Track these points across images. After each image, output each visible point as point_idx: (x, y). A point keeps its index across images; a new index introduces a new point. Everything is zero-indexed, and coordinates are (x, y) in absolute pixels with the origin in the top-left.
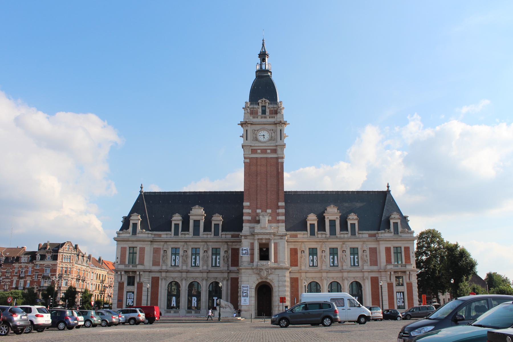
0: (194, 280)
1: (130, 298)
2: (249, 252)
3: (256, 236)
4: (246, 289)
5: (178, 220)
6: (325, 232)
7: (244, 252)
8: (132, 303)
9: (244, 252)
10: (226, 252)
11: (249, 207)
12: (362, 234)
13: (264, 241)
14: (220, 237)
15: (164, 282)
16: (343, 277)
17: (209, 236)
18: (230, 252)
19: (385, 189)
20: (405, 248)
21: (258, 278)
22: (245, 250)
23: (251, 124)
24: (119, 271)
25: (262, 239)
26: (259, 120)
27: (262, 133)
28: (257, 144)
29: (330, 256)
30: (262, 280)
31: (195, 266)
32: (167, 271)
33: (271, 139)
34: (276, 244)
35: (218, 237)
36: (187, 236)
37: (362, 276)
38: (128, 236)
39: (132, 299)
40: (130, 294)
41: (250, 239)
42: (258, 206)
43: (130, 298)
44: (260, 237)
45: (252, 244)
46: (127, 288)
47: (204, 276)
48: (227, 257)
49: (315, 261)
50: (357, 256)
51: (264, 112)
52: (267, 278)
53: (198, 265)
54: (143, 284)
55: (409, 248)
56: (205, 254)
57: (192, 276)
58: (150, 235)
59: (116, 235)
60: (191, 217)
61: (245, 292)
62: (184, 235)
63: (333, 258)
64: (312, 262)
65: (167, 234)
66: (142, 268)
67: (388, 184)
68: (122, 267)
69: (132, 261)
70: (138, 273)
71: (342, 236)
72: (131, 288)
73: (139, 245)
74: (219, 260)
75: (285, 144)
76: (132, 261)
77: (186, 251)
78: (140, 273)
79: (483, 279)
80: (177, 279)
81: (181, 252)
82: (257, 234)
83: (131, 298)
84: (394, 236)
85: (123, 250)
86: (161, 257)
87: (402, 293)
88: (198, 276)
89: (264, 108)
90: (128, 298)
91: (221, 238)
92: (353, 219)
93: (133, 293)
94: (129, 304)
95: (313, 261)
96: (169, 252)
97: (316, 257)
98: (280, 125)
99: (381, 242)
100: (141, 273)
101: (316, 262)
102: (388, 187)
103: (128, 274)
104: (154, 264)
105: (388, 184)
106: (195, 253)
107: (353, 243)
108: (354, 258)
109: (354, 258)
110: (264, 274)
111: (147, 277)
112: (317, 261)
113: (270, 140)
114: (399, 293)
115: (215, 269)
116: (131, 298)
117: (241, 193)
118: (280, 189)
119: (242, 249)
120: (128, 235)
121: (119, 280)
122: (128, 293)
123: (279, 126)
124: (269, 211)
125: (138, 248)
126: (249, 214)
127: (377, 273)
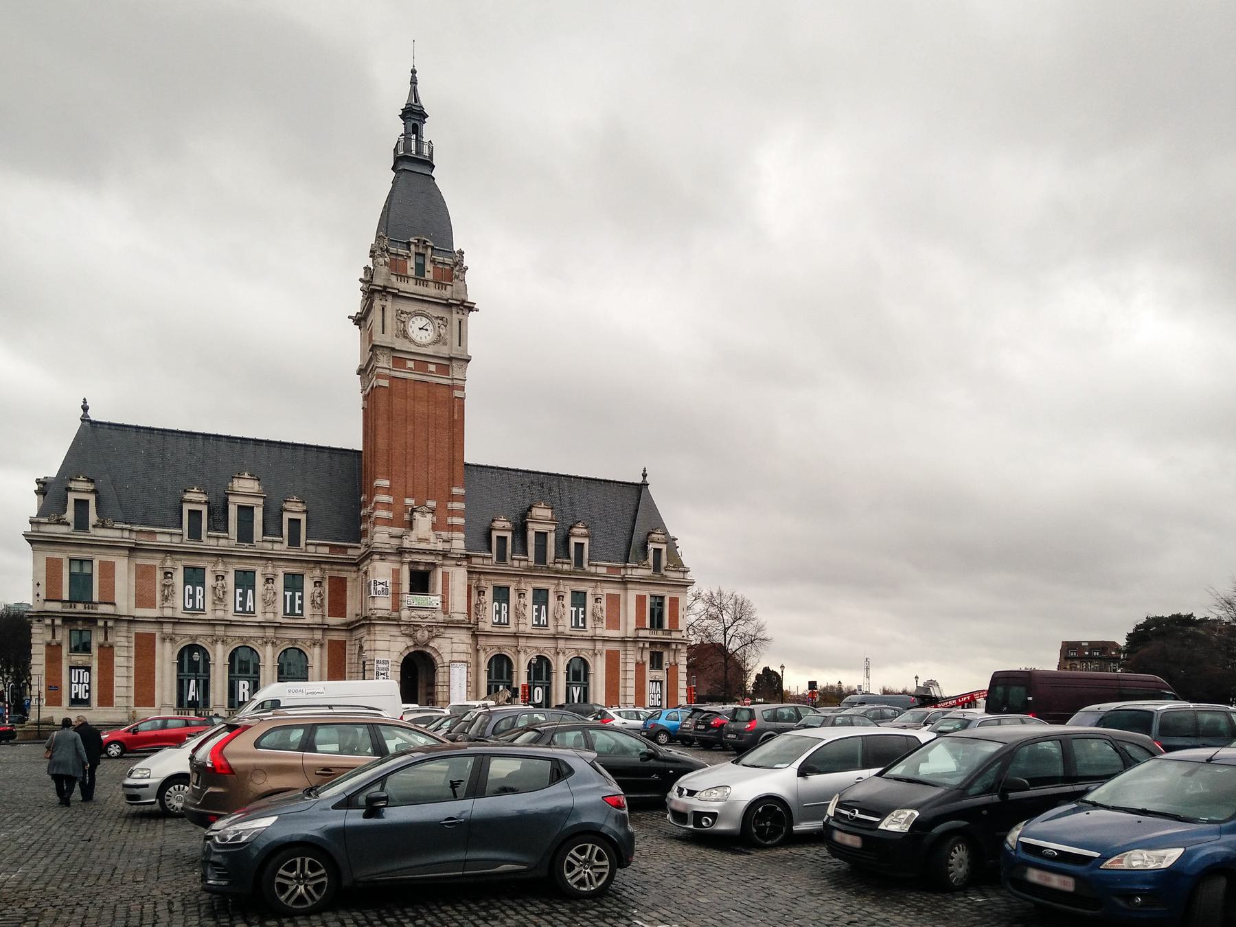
0: (244, 643)
1: (78, 683)
2: (390, 590)
3: (407, 555)
4: (385, 666)
5: (199, 503)
6: (227, 534)
7: (379, 588)
8: (87, 694)
9: (379, 588)
10: (317, 584)
11: (388, 491)
12: (597, 565)
13: (421, 568)
14: (304, 551)
15: (168, 645)
16: (556, 648)
17: (277, 546)
18: (326, 585)
19: (639, 480)
20: (671, 599)
21: (411, 643)
22: (380, 584)
23: (395, 296)
24: (49, 616)
25: (418, 563)
26: (410, 287)
27: (420, 322)
28: (406, 345)
29: (237, 590)
30: (416, 649)
31: (244, 611)
32: (177, 622)
33: (439, 340)
34: (445, 575)
35: (297, 550)
36: (222, 542)
37: (592, 647)
38: (67, 532)
39: (84, 685)
40: (79, 673)
41: (392, 562)
42: (410, 490)
43: (78, 683)
44: (416, 558)
45: (396, 573)
46: (650, 674)
47: (316, 637)
48: (320, 595)
49: (199, 597)
50: (583, 609)
51: (420, 269)
52: (427, 645)
53: (252, 610)
54: (115, 649)
55: (678, 601)
56: (270, 586)
57: (238, 634)
58: (126, 534)
59: (28, 528)
60: (530, 525)
61: (383, 672)
62: (215, 540)
63: (538, 610)
64: (191, 600)
65: (130, 531)
66: (112, 612)
67: (645, 471)
68: (56, 607)
69: (657, 623)
70: (101, 623)
71: (559, 566)
72: (80, 658)
73: (98, 557)
74: (300, 602)
75: (470, 356)
76: (657, 623)
77: (223, 577)
78: (106, 623)
79: (1053, 667)
80: (299, 643)
81: (210, 580)
82: (411, 552)
83: (82, 681)
84: (287, 550)
85: (53, 568)
86: (158, 587)
87: (658, 683)
88: (252, 635)
89: (420, 260)
90: (73, 681)
91: (306, 551)
92: (504, 529)
93: (88, 669)
94: (77, 695)
95: (193, 596)
96: (179, 578)
97: (201, 589)
98: (460, 309)
99: (629, 586)
100: (110, 624)
101: (202, 599)
102: (644, 476)
103: (71, 626)
104: (139, 604)
105: (645, 471)
106: (293, 582)
107: (578, 583)
108: (577, 612)
109: (577, 612)
110: (422, 635)
111: (125, 634)
112: (204, 597)
113: (435, 342)
114: (654, 683)
115: (538, 632)
116: (83, 683)
117: (361, 452)
118: (457, 455)
119: (375, 582)
120: (62, 529)
121: (639, 658)
122: (73, 670)
123: (458, 313)
124: (432, 504)
125: (96, 563)
126: (388, 506)
127: (617, 644)
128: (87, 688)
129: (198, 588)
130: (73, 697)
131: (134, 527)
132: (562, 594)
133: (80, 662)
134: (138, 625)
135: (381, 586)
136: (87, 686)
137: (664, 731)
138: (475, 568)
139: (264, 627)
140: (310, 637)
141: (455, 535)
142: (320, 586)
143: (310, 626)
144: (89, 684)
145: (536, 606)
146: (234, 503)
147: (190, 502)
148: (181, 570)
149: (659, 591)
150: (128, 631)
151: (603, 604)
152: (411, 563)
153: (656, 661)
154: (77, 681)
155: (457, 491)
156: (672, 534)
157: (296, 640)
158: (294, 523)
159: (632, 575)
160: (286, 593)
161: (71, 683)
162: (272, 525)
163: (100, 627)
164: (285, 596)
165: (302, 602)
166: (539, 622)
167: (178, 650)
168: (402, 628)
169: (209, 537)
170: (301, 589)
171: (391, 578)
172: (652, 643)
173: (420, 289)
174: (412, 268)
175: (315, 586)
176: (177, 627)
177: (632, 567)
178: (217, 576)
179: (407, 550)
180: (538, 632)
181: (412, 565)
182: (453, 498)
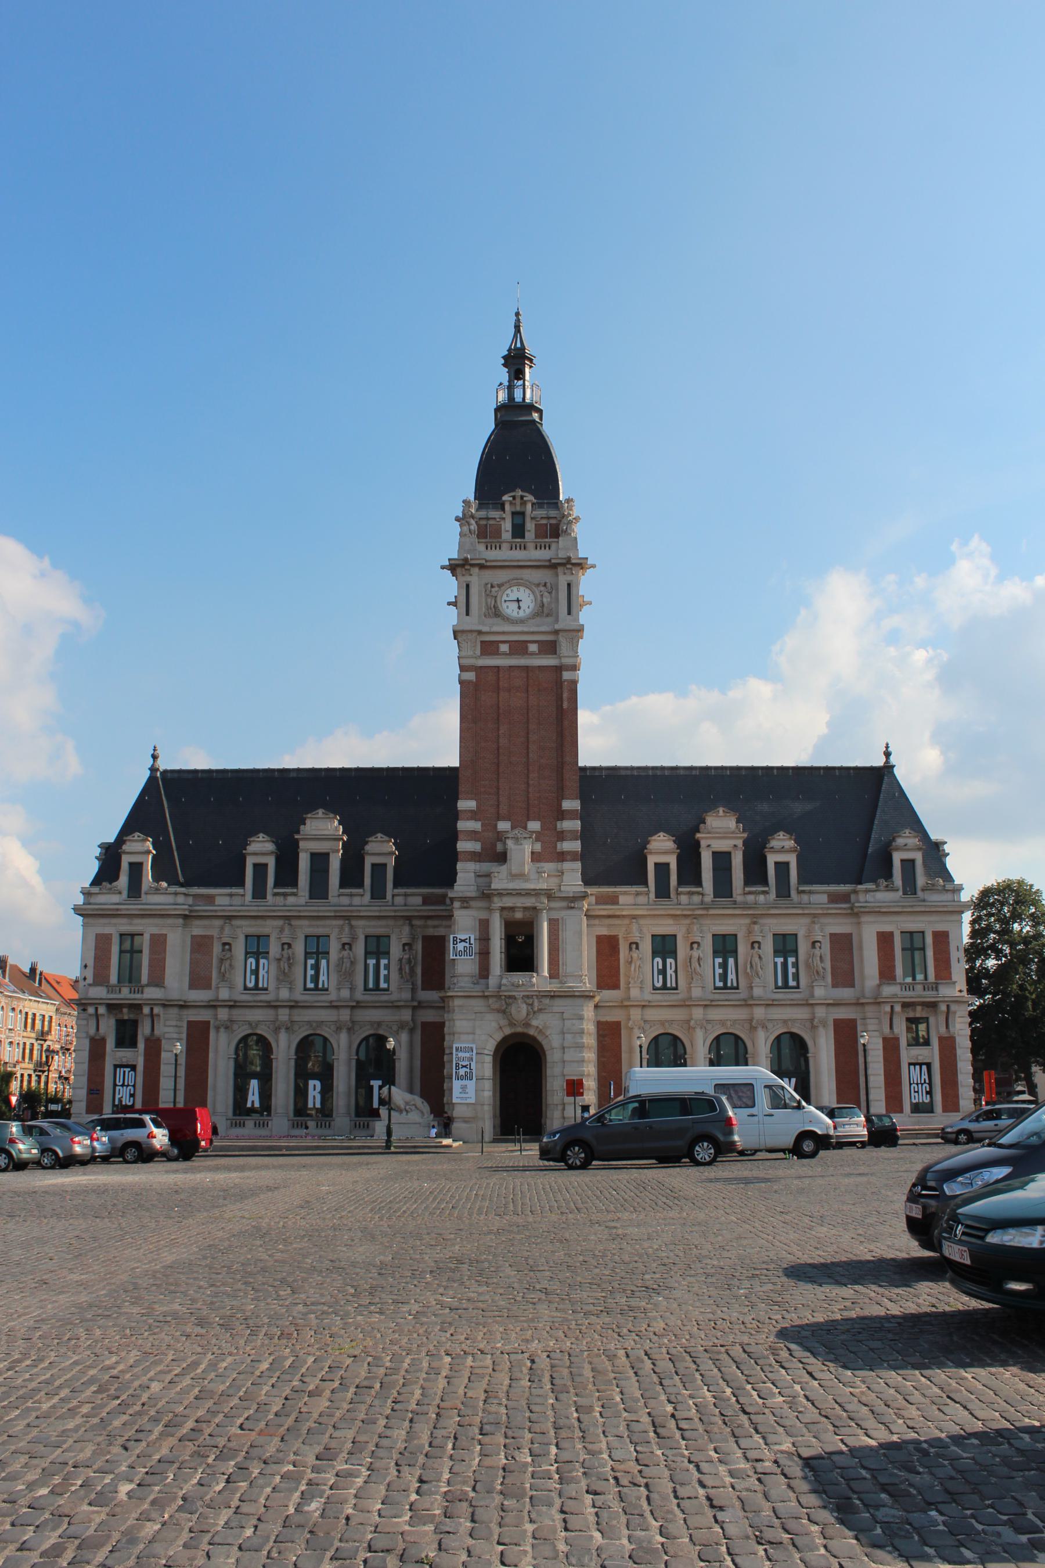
1: (123, 1085)
4: (467, 1055)
8: (132, 1099)
10: (406, 948)
11: (473, 815)
12: (810, 892)
13: (519, 915)
18: (419, 946)
19: (879, 761)
23: (482, 567)
25: (512, 909)
26: (504, 554)
29: (716, 959)
30: (513, 1031)
31: (316, 988)
32: (233, 1005)
34: (554, 924)
39: (129, 1088)
40: (124, 1072)
41: (479, 908)
43: (123, 1085)
44: (508, 902)
45: (484, 926)
47: (342, 1018)
49: (670, 972)
52: (527, 1025)
53: (326, 986)
54: (163, 1042)
56: (345, 953)
58: (181, 899)
59: (80, 900)
60: (302, 844)
61: (464, 1064)
62: (282, 898)
64: (661, 977)
67: (887, 747)
69: (130, 975)
70: (146, 1010)
72: (125, 1055)
73: (148, 928)
76: (130, 975)
78: (152, 1009)
81: (274, 949)
82: (500, 895)
83: (126, 1084)
85: (102, 944)
87: (924, 1067)
88: (323, 1018)
89: (518, 521)
90: (118, 1083)
91: (393, 905)
93: (133, 1068)
94: (120, 1101)
95: (663, 972)
96: (239, 949)
100: (156, 1010)
102: (887, 754)
104: (194, 985)
105: (887, 747)
106: (317, 949)
107: (782, 920)
108: (785, 965)
109: (785, 965)
110: (520, 1011)
111: (174, 1023)
114: (918, 1067)
115: (722, 997)
116: (128, 1085)
119: (455, 939)
122: (118, 1069)
128: (132, 1092)
129: (669, 961)
130: (117, 1103)
131: (190, 890)
132: (759, 939)
133: (124, 1060)
134: (191, 1011)
135: (463, 944)
136: (132, 1088)
137: (99, 1157)
138: (359, 911)
139: (336, 1007)
140: (396, 1018)
141: (567, 865)
142: (411, 949)
143: (396, 1004)
144: (134, 1086)
145: (720, 960)
146: (306, 851)
147: (255, 854)
148: (242, 939)
149: (913, 924)
150: (180, 1020)
151: (826, 948)
152: (503, 909)
153: (126, 1036)
154: (121, 1083)
155: (568, 805)
156: (934, 836)
157: (379, 1024)
158: (782, 868)
159: (866, 902)
160: (777, 959)
161: (115, 1085)
162: (756, 872)
163: (90, 1015)
164: (775, 964)
165: (389, 972)
166: (725, 983)
167: (772, 1037)
168: (491, 1001)
169: (275, 894)
170: (387, 954)
171: (477, 933)
172: (905, 1005)
173: (518, 555)
174: (508, 531)
175: (404, 950)
176: (296, 1011)
177: (867, 891)
178: (283, 944)
179: (496, 892)
180: (722, 997)
181: (505, 913)
182: (562, 815)
